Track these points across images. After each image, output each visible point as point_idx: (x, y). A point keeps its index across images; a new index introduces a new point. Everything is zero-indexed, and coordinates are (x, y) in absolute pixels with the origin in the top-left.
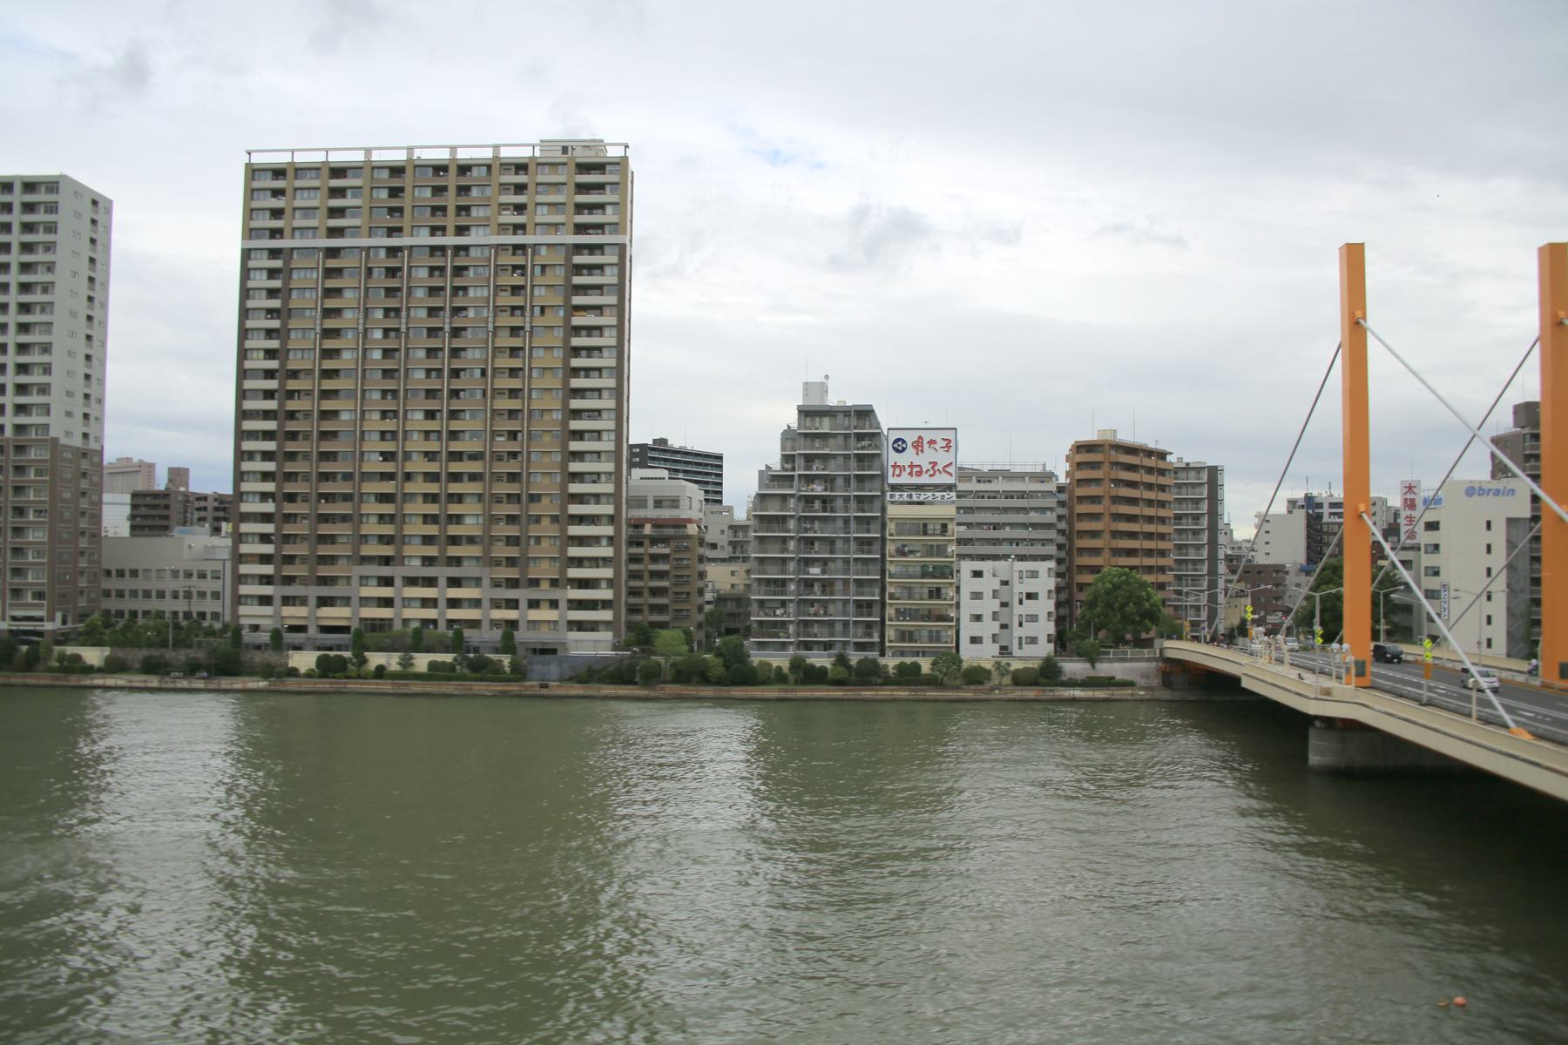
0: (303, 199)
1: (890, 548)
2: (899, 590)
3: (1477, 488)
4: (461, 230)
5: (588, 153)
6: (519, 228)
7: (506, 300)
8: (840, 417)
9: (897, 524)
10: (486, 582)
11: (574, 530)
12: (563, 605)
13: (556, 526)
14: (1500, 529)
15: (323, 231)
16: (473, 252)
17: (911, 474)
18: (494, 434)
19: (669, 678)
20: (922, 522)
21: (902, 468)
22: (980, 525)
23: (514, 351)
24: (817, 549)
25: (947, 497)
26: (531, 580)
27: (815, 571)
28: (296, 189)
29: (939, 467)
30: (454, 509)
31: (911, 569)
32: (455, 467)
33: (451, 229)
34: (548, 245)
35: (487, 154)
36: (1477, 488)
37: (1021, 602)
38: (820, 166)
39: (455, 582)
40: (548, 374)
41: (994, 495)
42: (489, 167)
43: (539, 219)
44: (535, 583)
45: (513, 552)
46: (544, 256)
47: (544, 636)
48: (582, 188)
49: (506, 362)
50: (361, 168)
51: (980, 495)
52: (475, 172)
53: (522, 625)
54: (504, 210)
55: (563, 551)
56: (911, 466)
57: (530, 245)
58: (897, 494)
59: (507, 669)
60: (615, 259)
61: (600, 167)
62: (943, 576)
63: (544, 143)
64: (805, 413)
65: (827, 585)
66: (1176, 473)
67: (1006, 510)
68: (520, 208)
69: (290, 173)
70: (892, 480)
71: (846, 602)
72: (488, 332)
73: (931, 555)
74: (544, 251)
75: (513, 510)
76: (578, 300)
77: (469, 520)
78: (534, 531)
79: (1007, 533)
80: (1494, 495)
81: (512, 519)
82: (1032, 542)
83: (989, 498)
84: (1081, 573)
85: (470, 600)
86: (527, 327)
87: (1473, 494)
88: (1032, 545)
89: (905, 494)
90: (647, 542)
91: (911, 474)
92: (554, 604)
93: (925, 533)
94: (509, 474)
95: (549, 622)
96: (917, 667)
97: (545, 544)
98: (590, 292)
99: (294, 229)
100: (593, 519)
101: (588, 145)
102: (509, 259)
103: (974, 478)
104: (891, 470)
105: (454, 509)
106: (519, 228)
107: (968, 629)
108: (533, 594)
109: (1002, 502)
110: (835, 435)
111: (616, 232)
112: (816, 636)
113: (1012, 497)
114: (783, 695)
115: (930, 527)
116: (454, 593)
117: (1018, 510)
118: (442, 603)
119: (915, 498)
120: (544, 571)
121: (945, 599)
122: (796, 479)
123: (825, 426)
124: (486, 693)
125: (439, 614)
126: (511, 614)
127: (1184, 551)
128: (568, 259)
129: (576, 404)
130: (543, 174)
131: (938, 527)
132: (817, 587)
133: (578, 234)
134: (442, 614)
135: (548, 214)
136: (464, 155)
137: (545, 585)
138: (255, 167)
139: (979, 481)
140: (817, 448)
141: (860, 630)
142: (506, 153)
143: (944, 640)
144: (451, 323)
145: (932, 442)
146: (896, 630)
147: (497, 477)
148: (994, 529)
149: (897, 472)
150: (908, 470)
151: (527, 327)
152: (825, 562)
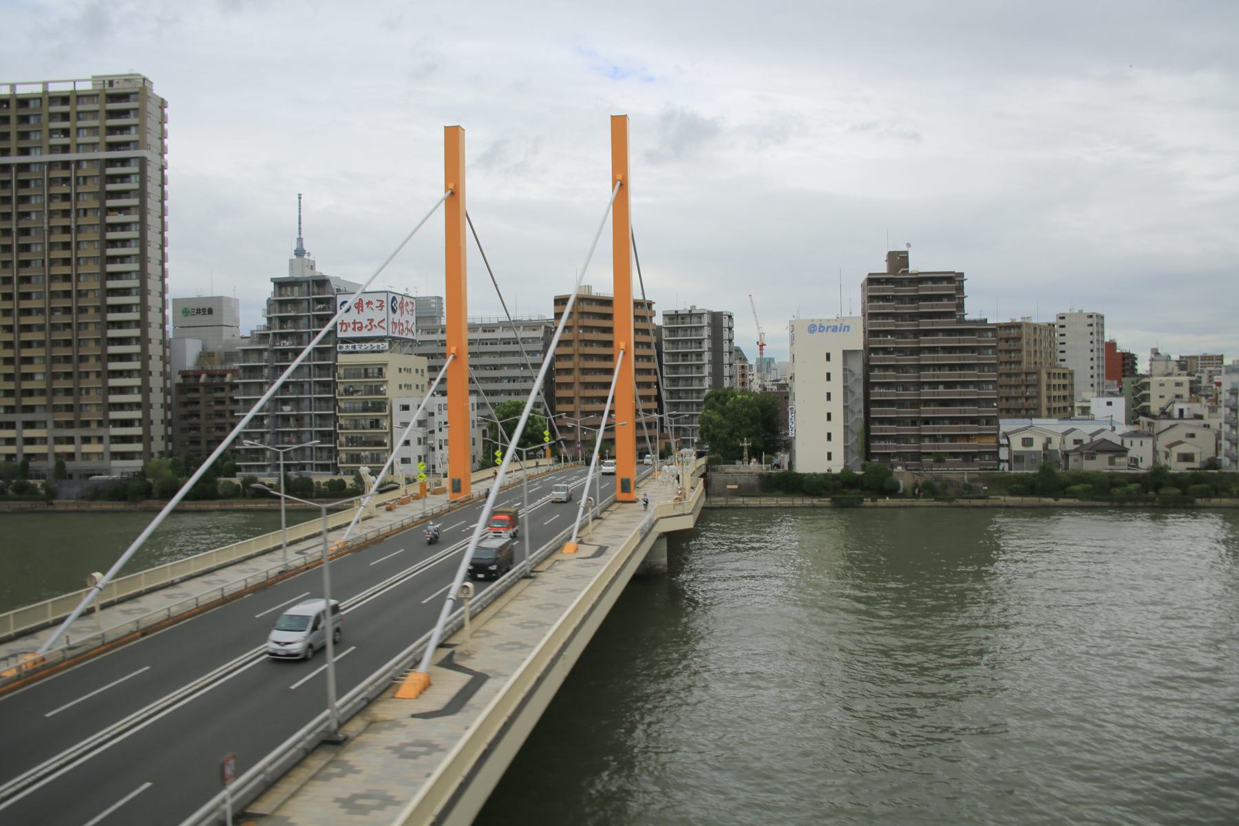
0: (83, 136)
1: (341, 388)
2: (348, 422)
3: (818, 325)
4: (25, 151)
5: (127, 85)
6: (65, 149)
7: (59, 205)
8: (305, 287)
9: (345, 370)
10: (50, 425)
11: (114, 382)
12: (106, 440)
13: (100, 380)
14: (837, 358)
15: (103, 146)
16: (33, 168)
17: (354, 329)
18: (53, 310)
19: (157, 496)
20: (364, 367)
22: (484, 367)
23: (66, 246)
24: (291, 391)
25: (381, 346)
26: (82, 422)
27: (287, 409)
28: (78, 129)
29: (375, 323)
30: (26, 369)
31: (357, 405)
32: (26, 337)
33: (14, 150)
34: (89, 161)
35: (38, 89)
36: (818, 325)
38: (650, 79)
39: (30, 425)
40: (91, 263)
41: (494, 342)
42: (41, 99)
43: (80, 140)
44: (86, 424)
45: (69, 401)
46: (86, 170)
47: (94, 463)
48: (112, 114)
49: (60, 254)
50: (97, 95)
51: (484, 342)
52: (32, 104)
53: (78, 456)
54: (55, 134)
55: (106, 399)
56: (355, 323)
57: (73, 161)
58: (345, 345)
59: (43, 492)
60: (136, 169)
61: (124, 97)
62: (380, 410)
63: (95, 79)
64: (280, 284)
65: (299, 419)
66: (683, 318)
68: (66, 132)
69: (73, 100)
70: (340, 335)
71: (311, 432)
72: (44, 231)
73: (371, 393)
74: (85, 165)
75: (68, 368)
76: (111, 203)
77: (38, 377)
78: (84, 384)
79: (506, 372)
80: (832, 331)
81: (68, 375)
83: (491, 344)
84: (559, 403)
85: (41, 438)
86: (73, 226)
88: (525, 381)
89: (350, 345)
90: (227, 388)
91: (354, 329)
92: (100, 440)
93: (366, 376)
94: (65, 340)
95: (98, 453)
96: (342, 483)
97: (93, 393)
98: (123, 195)
99: (78, 145)
100: (129, 373)
101: (128, 79)
102: (59, 173)
103: (480, 329)
105: (26, 369)
106: (65, 149)
108: (85, 432)
109: (501, 348)
110: (300, 301)
111: (136, 148)
112: (292, 460)
113: (509, 343)
114: (223, 507)
115: (370, 371)
116: (29, 433)
117: (514, 353)
118: (19, 441)
119: (358, 349)
120: (92, 414)
121: (382, 429)
122: (271, 336)
123: (295, 294)
124: (7, 510)
125: (18, 450)
126: (69, 448)
127: (690, 382)
128: (102, 171)
129: (112, 284)
130: (83, 103)
131: (376, 371)
132: (291, 420)
133: (110, 150)
134: (20, 450)
135: (88, 135)
136: (22, 91)
137: (94, 425)
138: (78, 93)
139: (485, 331)
140: (290, 312)
141: (325, 454)
142: (53, 88)
143: (382, 461)
144: (17, 225)
145: (369, 303)
146: (347, 454)
147: (55, 343)
148: (495, 369)
150: (352, 326)
151: (73, 226)
152: (297, 401)
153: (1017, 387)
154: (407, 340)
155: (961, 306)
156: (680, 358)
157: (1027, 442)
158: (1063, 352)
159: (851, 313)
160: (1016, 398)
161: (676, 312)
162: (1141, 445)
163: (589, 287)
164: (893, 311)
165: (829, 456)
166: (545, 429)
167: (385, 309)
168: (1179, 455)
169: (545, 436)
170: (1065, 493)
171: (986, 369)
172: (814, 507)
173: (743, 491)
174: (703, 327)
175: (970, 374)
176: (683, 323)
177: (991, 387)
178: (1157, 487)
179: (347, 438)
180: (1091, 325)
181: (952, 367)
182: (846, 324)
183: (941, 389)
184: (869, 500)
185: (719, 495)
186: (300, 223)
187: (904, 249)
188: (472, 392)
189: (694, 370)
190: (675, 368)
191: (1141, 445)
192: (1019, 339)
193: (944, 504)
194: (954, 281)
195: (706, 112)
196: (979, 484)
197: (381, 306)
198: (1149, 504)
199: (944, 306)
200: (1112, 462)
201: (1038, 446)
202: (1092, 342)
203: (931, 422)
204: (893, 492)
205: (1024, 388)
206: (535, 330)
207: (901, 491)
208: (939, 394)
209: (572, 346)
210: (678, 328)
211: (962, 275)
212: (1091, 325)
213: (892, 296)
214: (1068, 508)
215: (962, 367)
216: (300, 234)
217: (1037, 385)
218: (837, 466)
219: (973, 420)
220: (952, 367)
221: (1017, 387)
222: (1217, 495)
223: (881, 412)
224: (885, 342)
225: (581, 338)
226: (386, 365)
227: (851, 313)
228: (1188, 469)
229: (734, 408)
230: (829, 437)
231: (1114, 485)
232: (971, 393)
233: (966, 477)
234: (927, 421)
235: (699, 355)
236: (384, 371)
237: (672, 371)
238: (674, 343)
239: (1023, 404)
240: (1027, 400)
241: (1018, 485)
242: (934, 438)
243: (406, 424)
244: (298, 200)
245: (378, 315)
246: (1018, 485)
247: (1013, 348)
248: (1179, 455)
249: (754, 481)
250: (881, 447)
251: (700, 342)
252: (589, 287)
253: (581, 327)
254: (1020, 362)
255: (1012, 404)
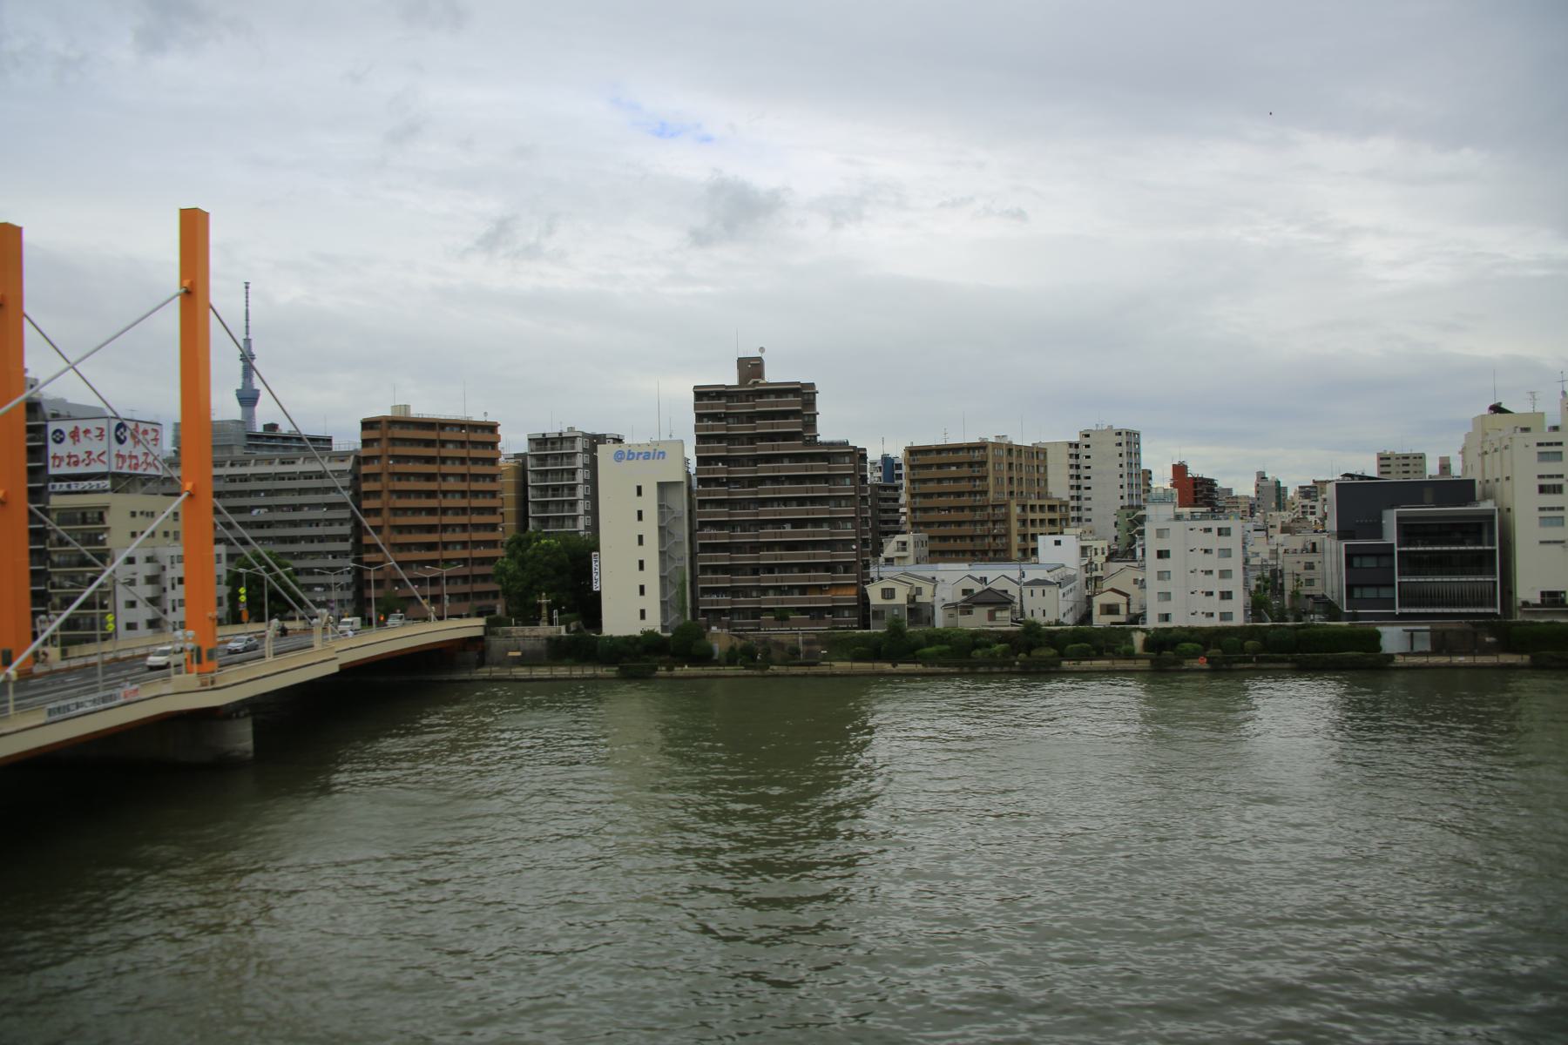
9: (59, 514)
14: (651, 493)
17: (69, 464)
21: (61, 459)
22: (280, 507)
25: (102, 485)
29: (94, 456)
37: (173, 587)
38: (708, 139)
41: (292, 477)
51: (280, 477)
58: (58, 484)
66: (553, 443)
67: (302, 491)
70: (52, 471)
80: (644, 458)
82: (330, 522)
83: (289, 479)
87: (622, 459)
89: (65, 484)
91: (69, 464)
93: (84, 522)
104: (51, 461)
107: (125, 615)
113: (311, 478)
115: (89, 515)
117: (317, 491)
119: (73, 488)
127: (561, 523)
131: (96, 515)
139: (283, 463)
145: (87, 432)
149: (57, 462)
150: (66, 460)
153: (983, 523)
154: (150, 478)
155: (811, 424)
156: (550, 492)
157: (888, 593)
158: (1089, 478)
159: (671, 436)
160: (983, 537)
161: (544, 435)
162: (1044, 595)
163: (407, 407)
164: (724, 432)
165: (643, 614)
166: (241, 586)
167: (105, 438)
168: (1102, 606)
169: (240, 595)
170: (915, 657)
171: (843, 503)
172: (595, 678)
173: (528, 660)
174: (576, 453)
175: (819, 511)
176: (553, 449)
177: (849, 525)
178: (1029, 648)
179: (61, 599)
180: (1120, 444)
181: (801, 501)
182: (659, 449)
183: (788, 528)
184: (664, 668)
185: (498, 664)
186: (247, 320)
187: (757, 354)
188: (218, 541)
189: (566, 507)
190: (544, 506)
191: (1044, 595)
192: (983, 463)
193: (756, 673)
194: (804, 395)
195: (762, 179)
196: (817, 648)
197: (101, 435)
198: (1006, 669)
199: (792, 425)
200: (992, 617)
201: (901, 598)
202: (1121, 466)
203: (776, 570)
204: (705, 658)
205: (990, 525)
206: (343, 461)
207: (716, 657)
208: (788, 535)
209: (380, 480)
210: (547, 455)
211: (812, 385)
212: (1120, 444)
213: (725, 413)
214: (910, 676)
215: (813, 500)
216: (247, 333)
217: (1005, 520)
218: (654, 622)
219: (829, 567)
220: (801, 501)
221: (983, 523)
222: (1100, 655)
223: (711, 559)
224: (714, 471)
225: (391, 471)
226: (107, 508)
227: (671, 436)
228: (1113, 623)
229: (533, 557)
230: (642, 590)
231: (976, 646)
232: (823, 533)
233: (800, 638)
234: (770, 569)
235: (573, 488)
236: (105, 515)
237: (540, 509)
238: (544, 474)
239: (989, 543)
240: (994, 540)
241: (862, 648)
242: (779, 590)
243: (132, 582)
244: (244, 290)
245: (97, 447)
246: (862, 648)
247: (976, 474)
248: (1102, 606)
249: (540, 646)
250: (712, 602)
251: (573, 472)
252: (407, 407)
253: (392, 457)
254: (984, 493)
255: (978, 545)
